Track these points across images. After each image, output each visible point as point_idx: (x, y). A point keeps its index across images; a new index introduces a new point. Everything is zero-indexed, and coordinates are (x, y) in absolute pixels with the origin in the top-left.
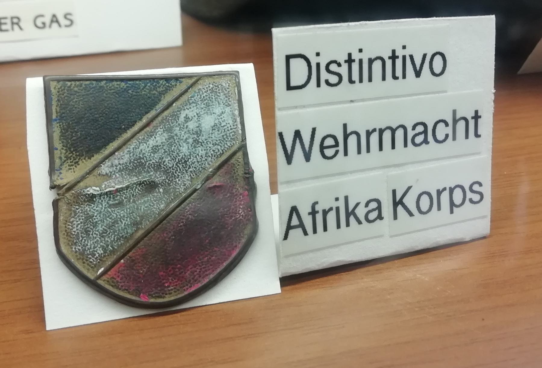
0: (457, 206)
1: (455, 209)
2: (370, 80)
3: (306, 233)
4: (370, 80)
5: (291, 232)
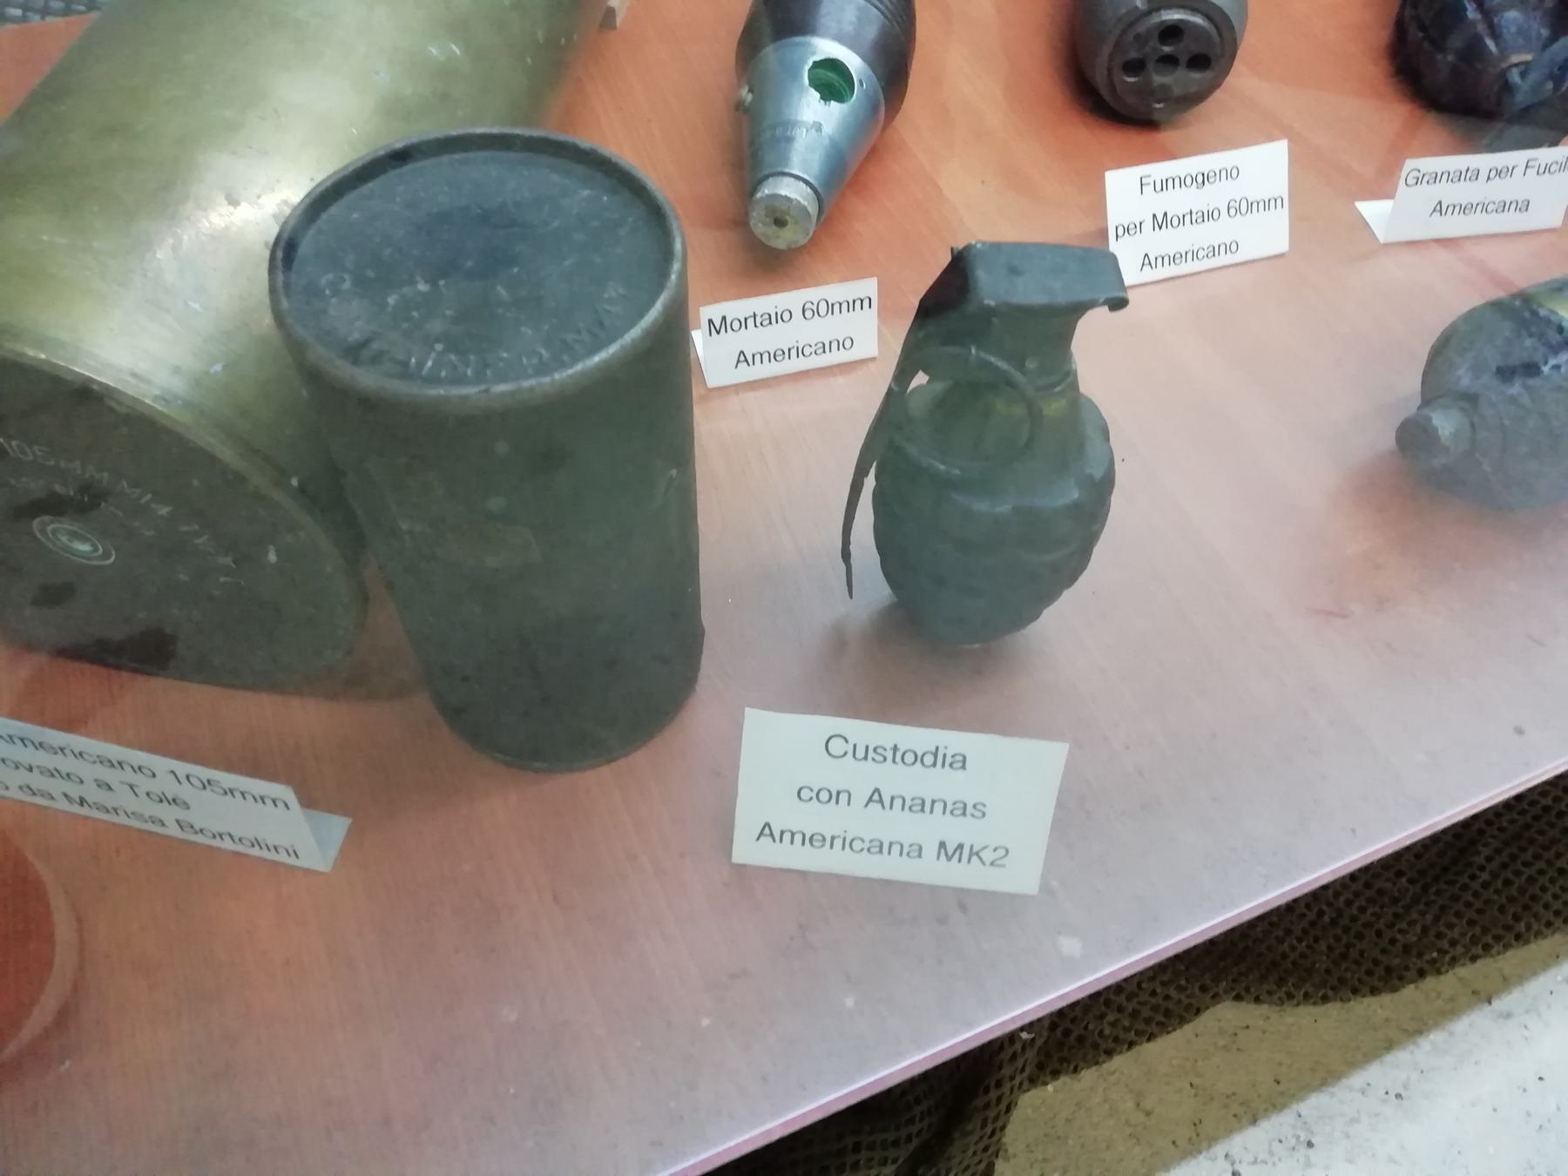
0: (931, 753)
1: (934, 750)
2: (854, 310)
3: (748, 364)
4: (854, 310)
5: (871, 804)
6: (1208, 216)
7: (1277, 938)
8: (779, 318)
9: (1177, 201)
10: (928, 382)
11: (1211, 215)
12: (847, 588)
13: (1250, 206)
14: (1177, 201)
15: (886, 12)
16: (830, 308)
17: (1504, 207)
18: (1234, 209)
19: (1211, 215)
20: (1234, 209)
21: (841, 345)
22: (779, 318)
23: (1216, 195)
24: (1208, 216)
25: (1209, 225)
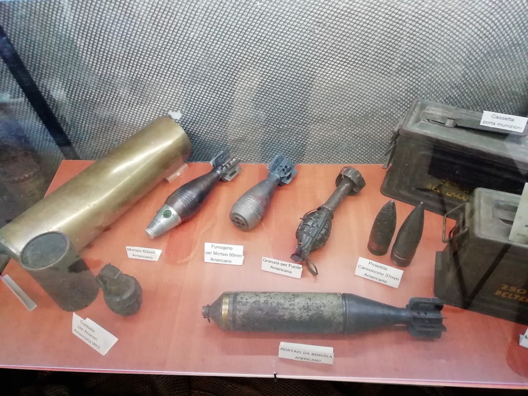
6: (226, 255)
7: (239, 312)
8: (139, 251)
9: (219, 251)
10: (244, 262)
11: (226, 255)
12: (495, 270)
13: (234, 255)
14: (219, 251)
15: (487, 169)
16: (148, 252)
17: (286, 271)
18: (231, 255)
19: (226, 255)
20: (231, 255)
21: (150, 258)
22: (139, 251)
23: (228, 252)
24: (226, 255)
25: (225, 257)
